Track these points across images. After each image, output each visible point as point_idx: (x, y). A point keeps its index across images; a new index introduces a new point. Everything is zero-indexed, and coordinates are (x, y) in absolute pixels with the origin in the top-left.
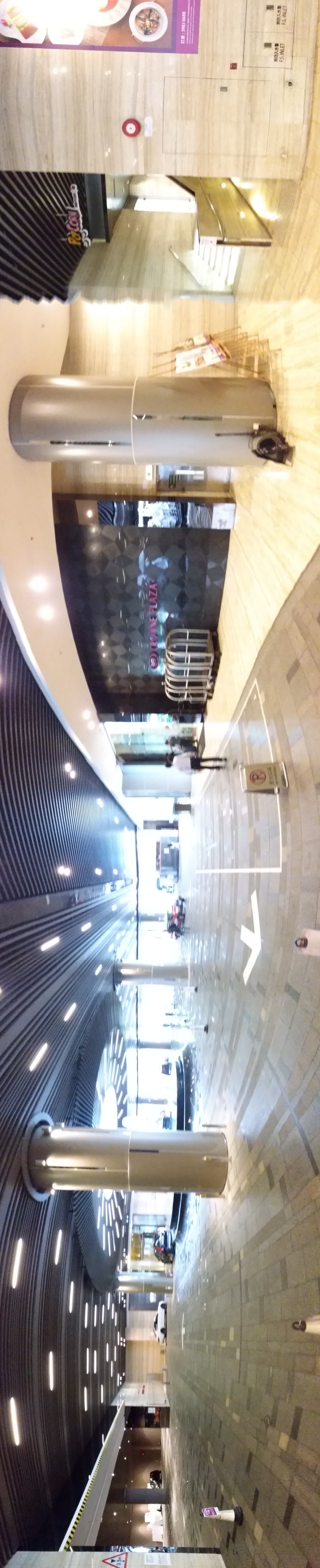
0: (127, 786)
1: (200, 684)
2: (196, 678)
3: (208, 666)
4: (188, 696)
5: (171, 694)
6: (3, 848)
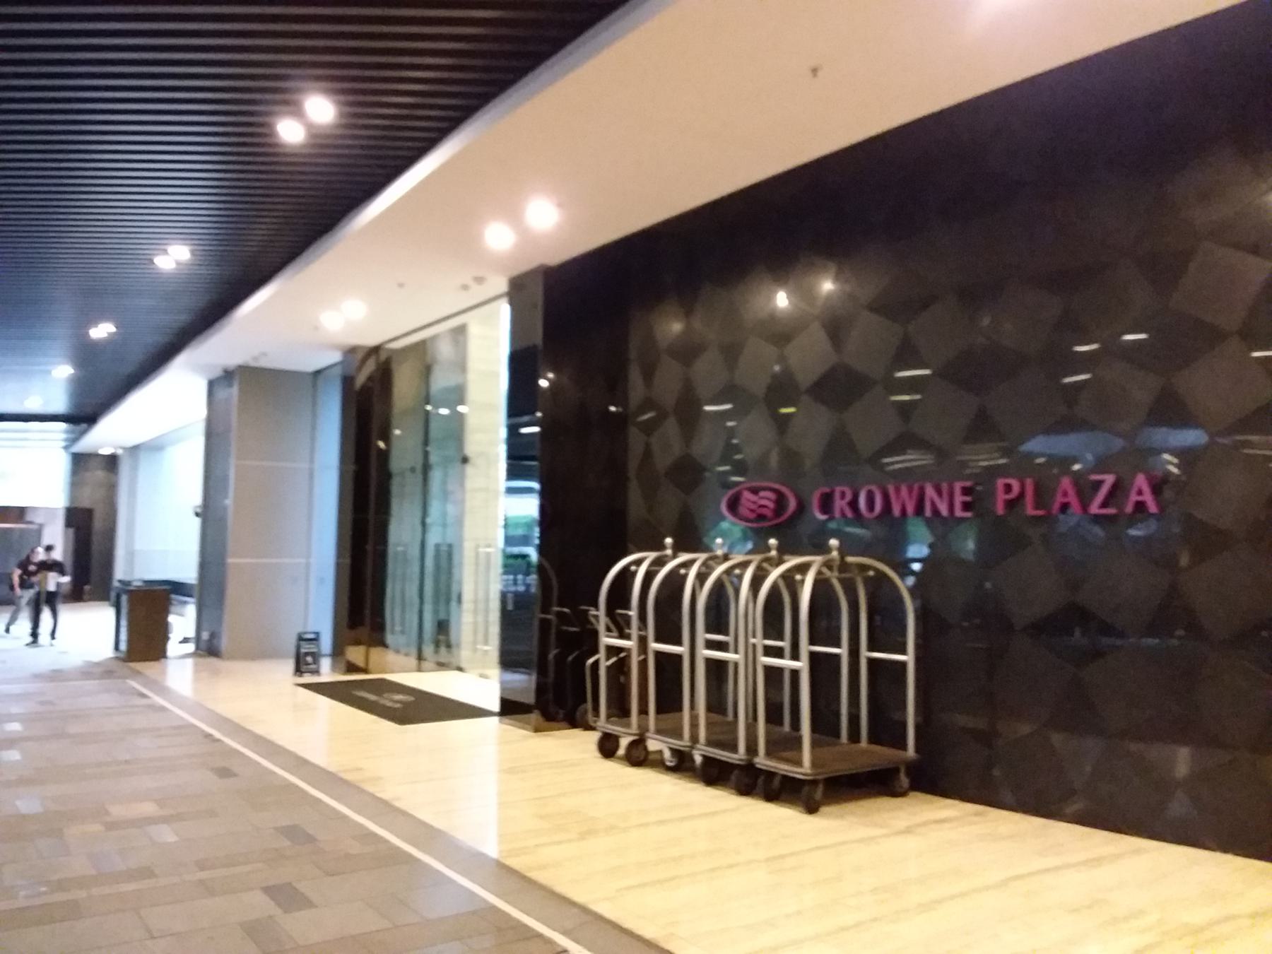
0: (252, 393)
1: (669, 701)
2: (696, 689)
3: (749, 737)
4: (612, 650)
5: (625, 577)
6: (142, 9)
